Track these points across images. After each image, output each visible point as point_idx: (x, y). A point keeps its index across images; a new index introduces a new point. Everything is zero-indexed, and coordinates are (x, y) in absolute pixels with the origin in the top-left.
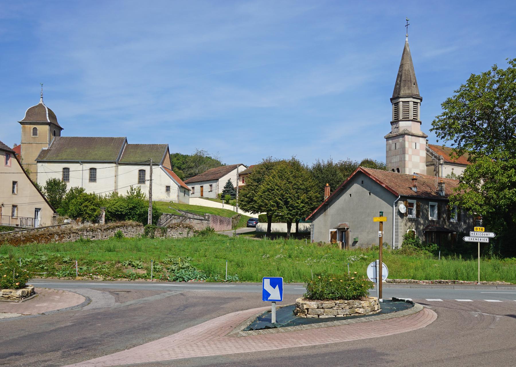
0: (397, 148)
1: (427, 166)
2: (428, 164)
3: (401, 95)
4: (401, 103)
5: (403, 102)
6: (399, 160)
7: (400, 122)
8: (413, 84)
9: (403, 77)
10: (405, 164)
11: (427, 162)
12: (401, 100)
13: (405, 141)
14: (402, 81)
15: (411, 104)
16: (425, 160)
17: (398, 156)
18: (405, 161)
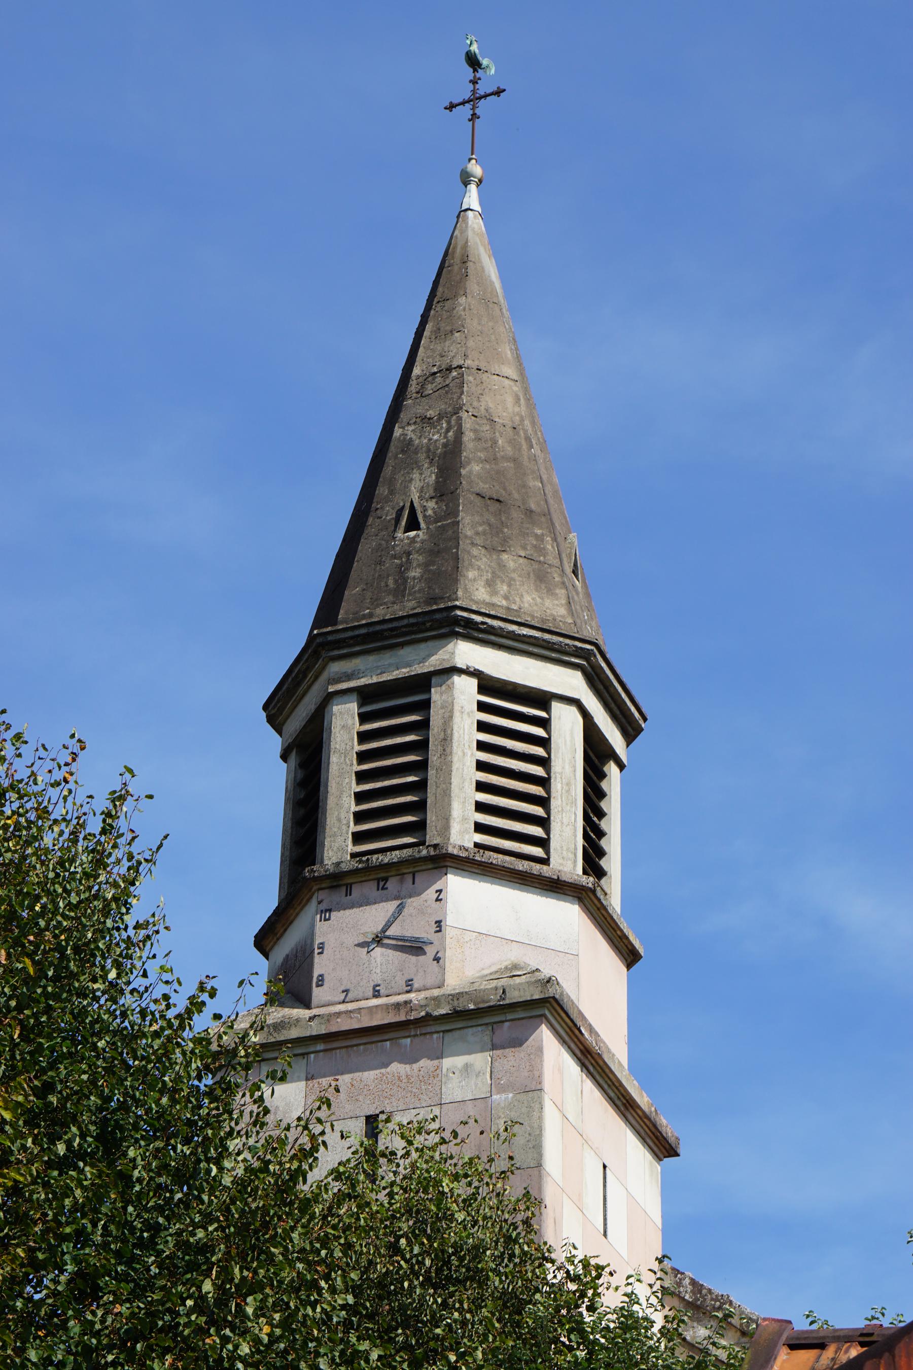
4: (465, 691)
7: (456, 885)
9: (473, 469)
12: (466, 653)
15: (566, 728)
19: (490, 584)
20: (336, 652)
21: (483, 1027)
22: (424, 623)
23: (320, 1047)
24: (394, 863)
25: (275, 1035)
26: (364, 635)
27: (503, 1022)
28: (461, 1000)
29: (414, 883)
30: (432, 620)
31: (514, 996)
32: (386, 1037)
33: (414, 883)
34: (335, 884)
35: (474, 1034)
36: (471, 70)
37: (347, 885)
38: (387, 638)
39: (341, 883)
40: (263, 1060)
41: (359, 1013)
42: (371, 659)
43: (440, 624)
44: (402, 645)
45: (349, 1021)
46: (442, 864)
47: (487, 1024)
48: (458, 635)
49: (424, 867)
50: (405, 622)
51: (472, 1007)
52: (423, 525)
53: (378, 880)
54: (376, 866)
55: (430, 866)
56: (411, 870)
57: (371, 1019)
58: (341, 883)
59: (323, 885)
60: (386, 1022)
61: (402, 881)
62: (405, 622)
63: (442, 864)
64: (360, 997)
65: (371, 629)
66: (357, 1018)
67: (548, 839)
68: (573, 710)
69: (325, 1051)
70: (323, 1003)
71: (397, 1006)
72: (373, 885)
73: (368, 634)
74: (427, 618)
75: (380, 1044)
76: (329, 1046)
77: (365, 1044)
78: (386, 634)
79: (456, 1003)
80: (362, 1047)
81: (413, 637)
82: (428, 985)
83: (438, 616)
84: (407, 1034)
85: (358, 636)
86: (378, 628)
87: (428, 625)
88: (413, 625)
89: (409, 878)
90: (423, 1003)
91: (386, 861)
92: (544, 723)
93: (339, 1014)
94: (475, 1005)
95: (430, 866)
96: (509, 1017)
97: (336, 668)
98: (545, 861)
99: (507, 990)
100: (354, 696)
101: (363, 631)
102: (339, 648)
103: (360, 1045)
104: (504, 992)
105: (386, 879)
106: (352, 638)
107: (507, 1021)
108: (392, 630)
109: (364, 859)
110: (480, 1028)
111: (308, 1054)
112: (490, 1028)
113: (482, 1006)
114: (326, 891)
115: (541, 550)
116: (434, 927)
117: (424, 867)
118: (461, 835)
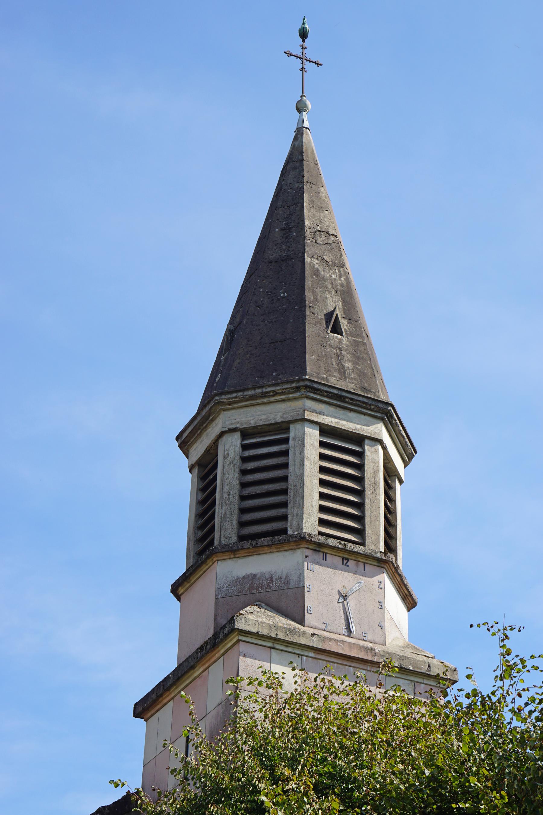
4: (312, 437)
20: (312, 395)
21: (409, 682)
22: (370, 405)
23: (312, 654)
24: (360, 553)
25: (290, 636)
26: (335, 394)
27: (420, 683)
28: (405, 661)
29: (364, 570)
30: (376, 406)
32: (353, 665)
33: (364, 570)
34: (318, 549)
36: (301, 40)
37: (323, 553)
38: (345, 402)
39: (321, 550)
40: (274, 648)
41: (343, 644)
42: (332, 409)
43: (379, 410)
44: (351, 410)
45: (336, 646)
46: (383, 565)
47: (411, 681)
48: (382, 419)
49: (371, 563)
50: (361, 399)
51: (411, 668)
52: (344, 334)
53: (343, 558)
54: (349, 551)
55: (376, 564)
56: (364, 561)
57: (351, 651)
58: (321, 550)
59: (310, 547)
60: (360, 657)
61: (357, 565)
62: (361, 399)
63: (383, 565)
64: (335, 631)
65: (340, 393)
66: (341, 646)
67: (364, 530)
68: (225, 438)
69: (395, 677)
70: (311, 625)
71: (366, 649)
72: (340, 560)
73: (337, 395)
74: (374, 403)
75: (347, 667)
76: (317, 656)
77: (338, 663)
78: (347, 400)
79: (402, 662)
80: (335, 664)
81: (360, 409)
82: (377, 640)
83: (380, 405)
84: (365, 668)
85: (331, 393)
86: (344, 394)
87: (372, 407)
88: (364, 403)
89: (361, 565)
90: (382, 653)
91: (356, 550)
92: (361, 455)
93: (330, 639)
94: (413, 667)
95: (376, 564)
96: (426, 682)
97: (309, 403)
98: (363, 544)
99: (431, 666)
100: (318, 428)
101: (335, 391)
102: (315, 393)
103: (335, 663)
104: (429, 666)
105: (348, 560)
106: (327, 392)
107: (423, 683)
108: (351, 399)
109: (343, 542)
110: (407, 682)
111: (302, 655)
112: (413, 684)
113: (417, 670)
114: (311, 551)
116: (377, 605)
117: (371, 563)
118: (310, 524)
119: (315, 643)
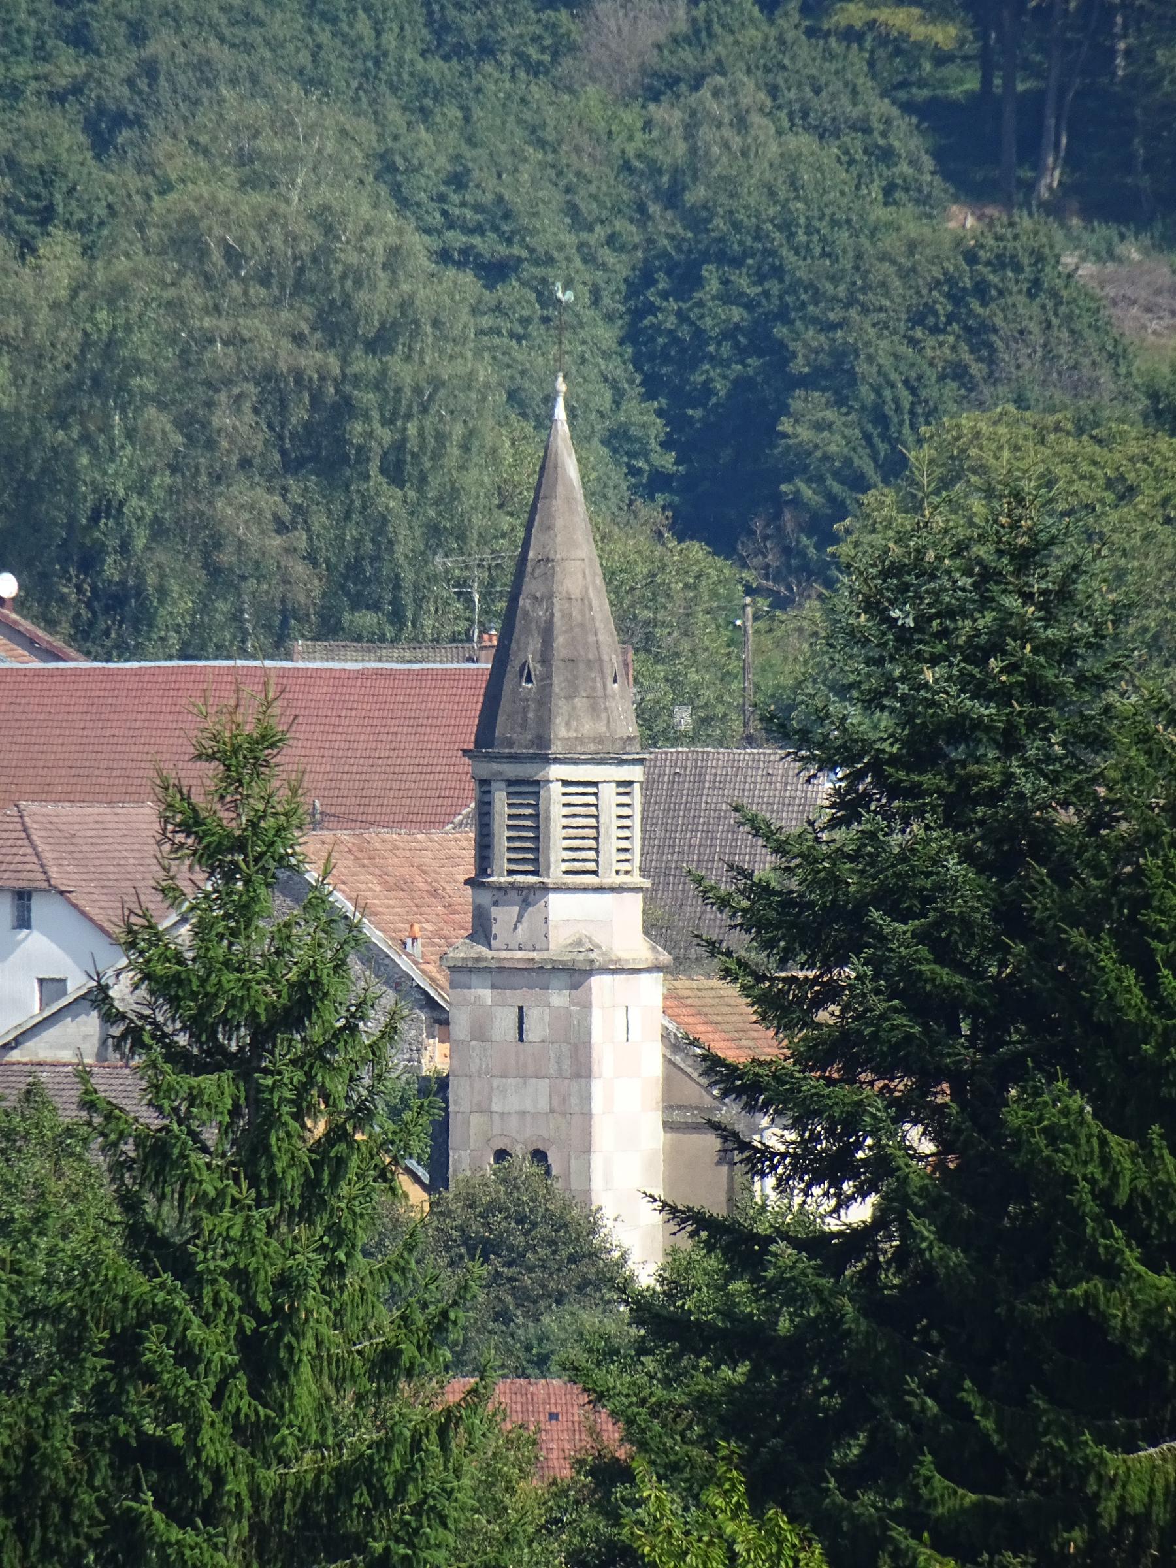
0: (531, 1035)
1: (669, 1126)
2: (677, 1116)
3: (556, 749)
5: (566, 783)
6: (543, 1104)
8: (610, 680)
9: (560, 641)
10: (587, 1134)
11: (669, 1107)
12: (557, 771)
13: (587, 1006)
14: (557, 664)
15: (609, 793)
16: (657, 1092)
17: (544, 1084)
18: (588, 1116)
19: (568, 724)
31: (579, 966)
35: (564, 978)
115: (594, 689)
119: (493, 964)
